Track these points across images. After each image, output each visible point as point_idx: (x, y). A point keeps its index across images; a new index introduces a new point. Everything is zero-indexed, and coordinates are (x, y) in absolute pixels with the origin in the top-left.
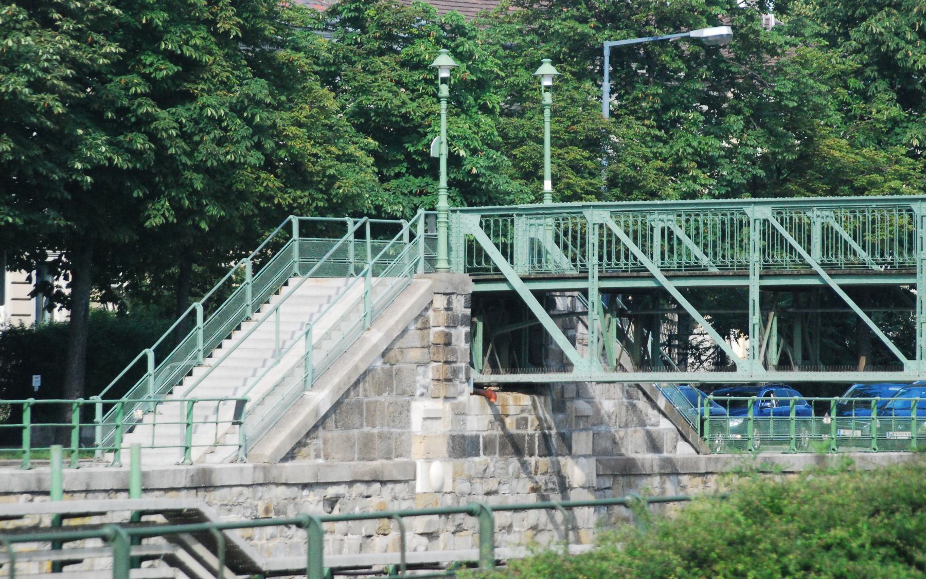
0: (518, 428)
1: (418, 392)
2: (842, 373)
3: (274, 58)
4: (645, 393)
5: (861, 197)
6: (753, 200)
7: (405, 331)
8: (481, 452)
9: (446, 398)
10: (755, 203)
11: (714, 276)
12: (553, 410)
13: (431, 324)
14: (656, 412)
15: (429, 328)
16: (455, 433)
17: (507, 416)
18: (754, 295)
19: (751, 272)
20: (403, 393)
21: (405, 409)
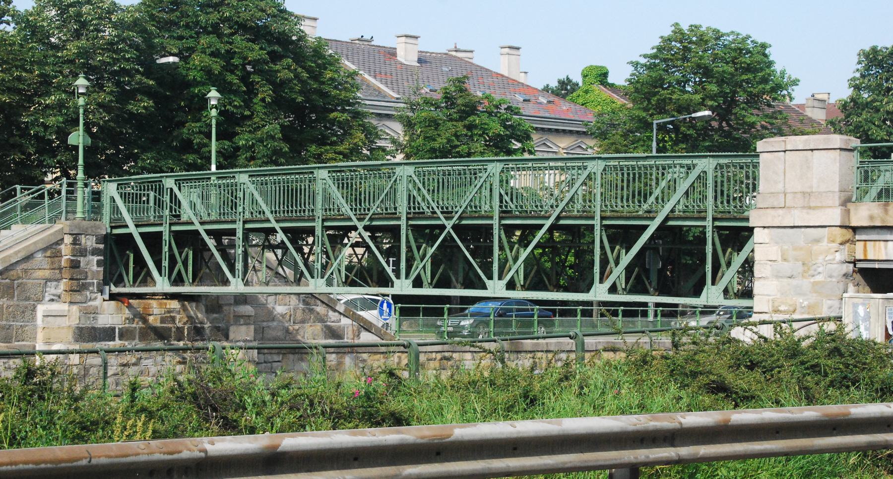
0: (161, 323)
1: (47, 299)
2: (217, 288)
3: (180, 58)
4: (323, 302)
5: (510, 158)
6: (496, 158)
7: (28, 258)
8: (117, 338)
9: (71, 303)
10: (319, 168)
11: (517, 217)
12: (207, 312)
13: (63, 254)
14: (337, 314)
15: (62, 256)
16: (80, 326)
17: (150, 315)
18: (166, 237)
19: (164, 222)
20: (28, 299)
21: (34, 309)
